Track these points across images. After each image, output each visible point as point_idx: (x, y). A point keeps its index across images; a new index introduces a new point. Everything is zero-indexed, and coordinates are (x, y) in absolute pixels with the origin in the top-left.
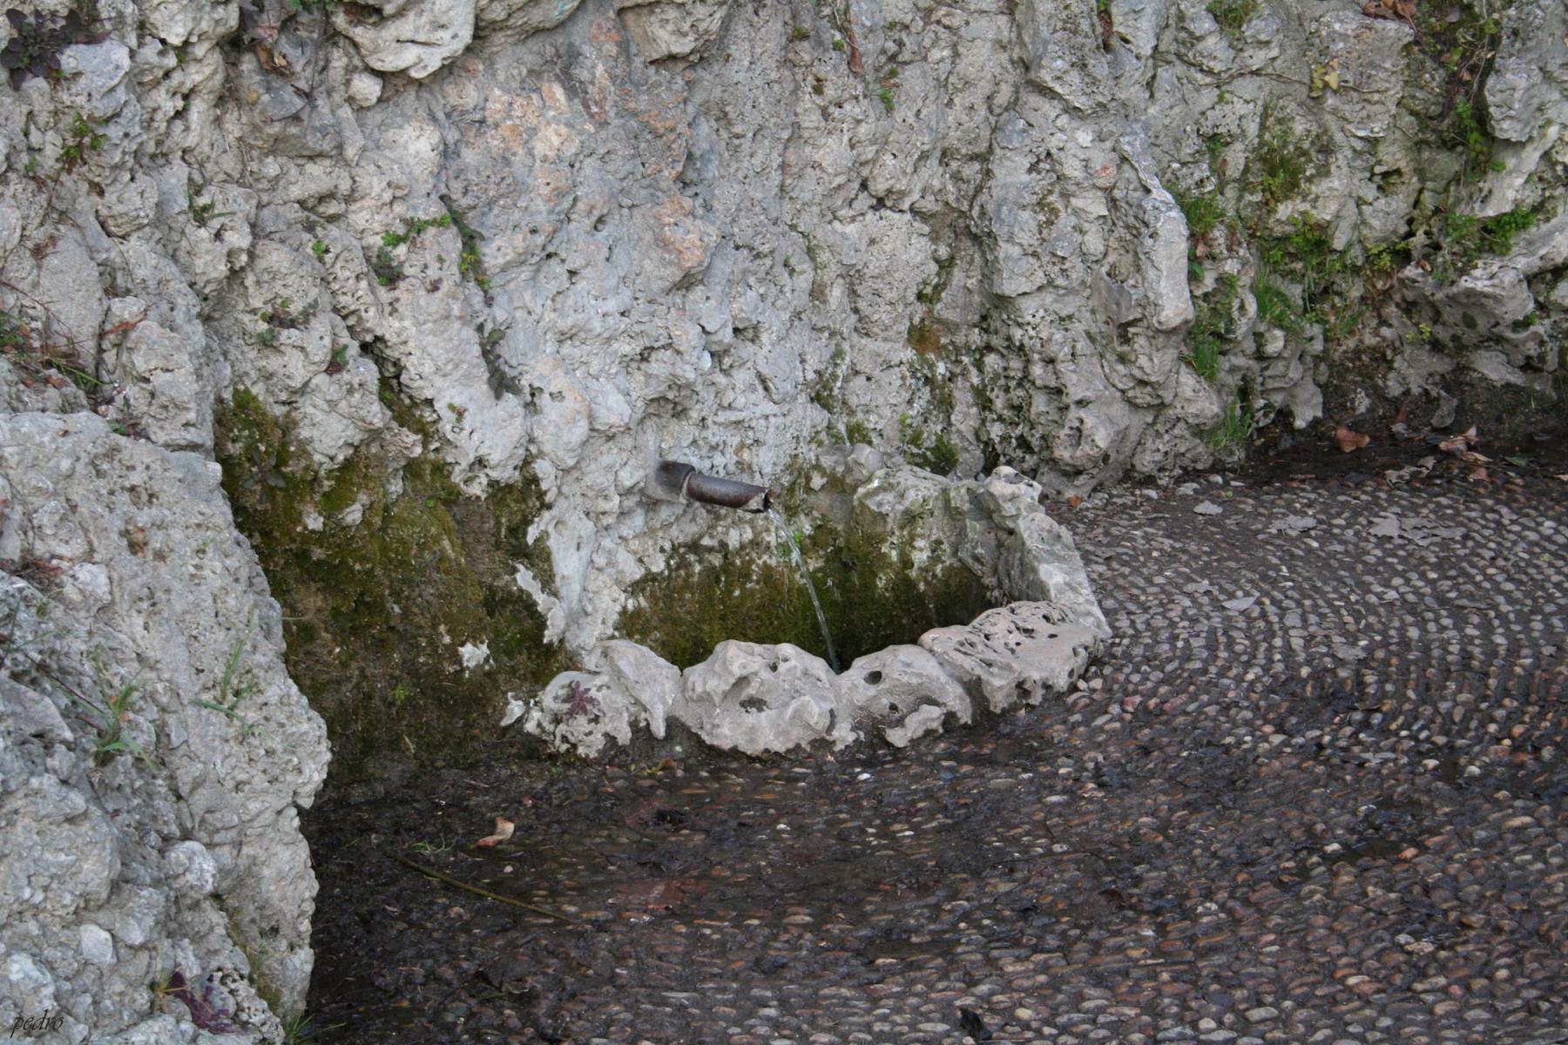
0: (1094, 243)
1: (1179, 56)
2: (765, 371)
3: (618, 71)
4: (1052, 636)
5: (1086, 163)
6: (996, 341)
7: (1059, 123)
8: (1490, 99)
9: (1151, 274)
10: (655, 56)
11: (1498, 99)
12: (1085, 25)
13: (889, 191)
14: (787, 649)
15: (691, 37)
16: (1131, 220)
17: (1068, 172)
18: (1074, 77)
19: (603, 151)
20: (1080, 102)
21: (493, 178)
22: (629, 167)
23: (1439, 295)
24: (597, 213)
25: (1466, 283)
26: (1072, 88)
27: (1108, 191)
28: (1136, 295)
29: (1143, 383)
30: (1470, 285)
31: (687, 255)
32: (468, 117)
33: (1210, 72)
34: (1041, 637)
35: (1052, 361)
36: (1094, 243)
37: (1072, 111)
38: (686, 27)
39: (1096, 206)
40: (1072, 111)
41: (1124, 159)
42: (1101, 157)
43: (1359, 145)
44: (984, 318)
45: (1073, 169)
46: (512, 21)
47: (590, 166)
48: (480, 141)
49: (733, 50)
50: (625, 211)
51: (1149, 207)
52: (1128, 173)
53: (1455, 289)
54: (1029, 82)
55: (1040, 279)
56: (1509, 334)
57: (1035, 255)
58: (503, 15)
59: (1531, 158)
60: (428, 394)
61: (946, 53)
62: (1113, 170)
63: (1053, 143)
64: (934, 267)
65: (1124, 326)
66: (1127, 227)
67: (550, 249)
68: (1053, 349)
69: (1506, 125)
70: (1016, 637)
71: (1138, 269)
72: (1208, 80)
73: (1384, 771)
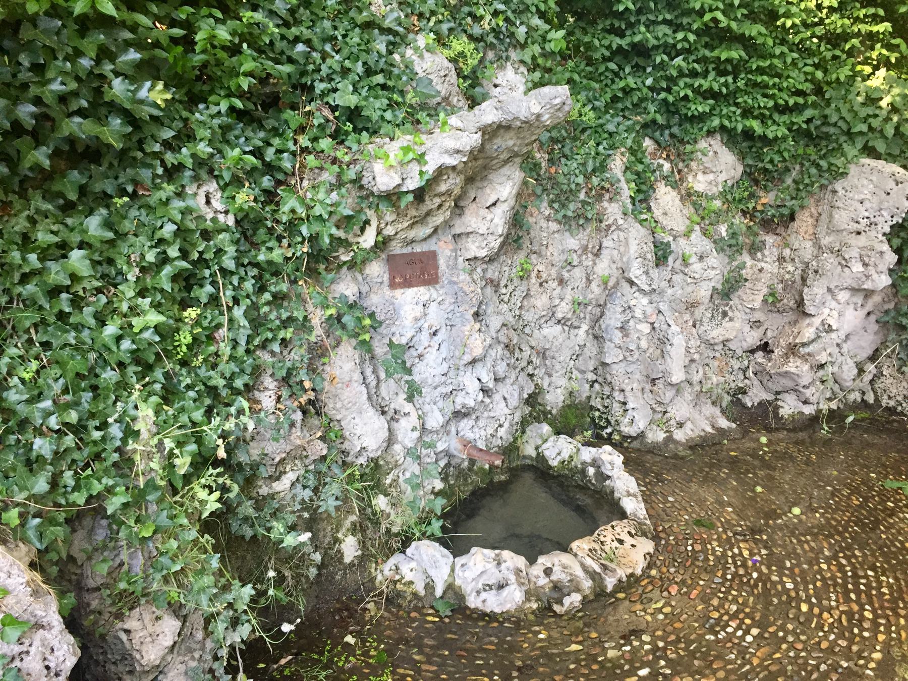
0: (644, 344)
1: (682, 271)
2: (506, 396)
3: (451, 263)
4: (633, 546)
5: (644, 312)
6: (600, 380)
7: (635, 295)
8: (805, 297)
9: (669, 360)
10: (469, 257)
11: (809, 297)
12: (649, 256)
13: (563, 318)
14: (506, 554)
15: (486, 250)
16: (661, 337)
17: (637, 315)
18: (644, 277)
19: (440, 299)
20: (646, 288)
21: (384, 311)
22: (452, 307)
23: (772, 372)
24: (434, 329)
25: (785, 368)
26: (642, 282)
27: (652, 324)
28: (661, 368)
29: (660, 403)
30: (788, 369)
31: (475, 350)
32: (375, 280)
33: (694, 278)
34: (627, 545)
35: (623, 391)
36: (644, 344)
37: (641, 291)
38: (484, 245)
39: (645, 328)
40: (641, 291)
41: (660, 312)
42: (650, 310)
43: (748, 311)
44: (595, 369)
45: (638, 314)
46: (398, 236)
47: (433, 307)
48: (380, 291)
49: (665, 241)
50: (449, 327)
51: (670, 333)
52: (661, 317)
53: (781, 370)
54: (624, 278)
55: (621, 358)
56: (801, 389)
57: (620, 347)
58: (393, 233)
59: (817, 321)
60: (338, 418)
61: (591, 263)
62: (655, 316)
63: (632, 303)
64: (578, 348)
65: (654, 380)
66: (659, 339)
67: (411, 344)
68: (624, 386)
69: (811, 308)
70: (616, 544)
71: (663, 357)
72: (692, 281)
73: (401, 115)
